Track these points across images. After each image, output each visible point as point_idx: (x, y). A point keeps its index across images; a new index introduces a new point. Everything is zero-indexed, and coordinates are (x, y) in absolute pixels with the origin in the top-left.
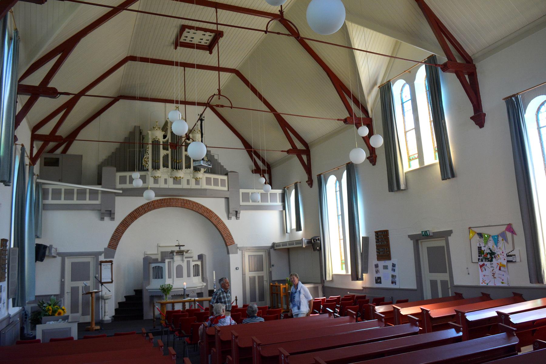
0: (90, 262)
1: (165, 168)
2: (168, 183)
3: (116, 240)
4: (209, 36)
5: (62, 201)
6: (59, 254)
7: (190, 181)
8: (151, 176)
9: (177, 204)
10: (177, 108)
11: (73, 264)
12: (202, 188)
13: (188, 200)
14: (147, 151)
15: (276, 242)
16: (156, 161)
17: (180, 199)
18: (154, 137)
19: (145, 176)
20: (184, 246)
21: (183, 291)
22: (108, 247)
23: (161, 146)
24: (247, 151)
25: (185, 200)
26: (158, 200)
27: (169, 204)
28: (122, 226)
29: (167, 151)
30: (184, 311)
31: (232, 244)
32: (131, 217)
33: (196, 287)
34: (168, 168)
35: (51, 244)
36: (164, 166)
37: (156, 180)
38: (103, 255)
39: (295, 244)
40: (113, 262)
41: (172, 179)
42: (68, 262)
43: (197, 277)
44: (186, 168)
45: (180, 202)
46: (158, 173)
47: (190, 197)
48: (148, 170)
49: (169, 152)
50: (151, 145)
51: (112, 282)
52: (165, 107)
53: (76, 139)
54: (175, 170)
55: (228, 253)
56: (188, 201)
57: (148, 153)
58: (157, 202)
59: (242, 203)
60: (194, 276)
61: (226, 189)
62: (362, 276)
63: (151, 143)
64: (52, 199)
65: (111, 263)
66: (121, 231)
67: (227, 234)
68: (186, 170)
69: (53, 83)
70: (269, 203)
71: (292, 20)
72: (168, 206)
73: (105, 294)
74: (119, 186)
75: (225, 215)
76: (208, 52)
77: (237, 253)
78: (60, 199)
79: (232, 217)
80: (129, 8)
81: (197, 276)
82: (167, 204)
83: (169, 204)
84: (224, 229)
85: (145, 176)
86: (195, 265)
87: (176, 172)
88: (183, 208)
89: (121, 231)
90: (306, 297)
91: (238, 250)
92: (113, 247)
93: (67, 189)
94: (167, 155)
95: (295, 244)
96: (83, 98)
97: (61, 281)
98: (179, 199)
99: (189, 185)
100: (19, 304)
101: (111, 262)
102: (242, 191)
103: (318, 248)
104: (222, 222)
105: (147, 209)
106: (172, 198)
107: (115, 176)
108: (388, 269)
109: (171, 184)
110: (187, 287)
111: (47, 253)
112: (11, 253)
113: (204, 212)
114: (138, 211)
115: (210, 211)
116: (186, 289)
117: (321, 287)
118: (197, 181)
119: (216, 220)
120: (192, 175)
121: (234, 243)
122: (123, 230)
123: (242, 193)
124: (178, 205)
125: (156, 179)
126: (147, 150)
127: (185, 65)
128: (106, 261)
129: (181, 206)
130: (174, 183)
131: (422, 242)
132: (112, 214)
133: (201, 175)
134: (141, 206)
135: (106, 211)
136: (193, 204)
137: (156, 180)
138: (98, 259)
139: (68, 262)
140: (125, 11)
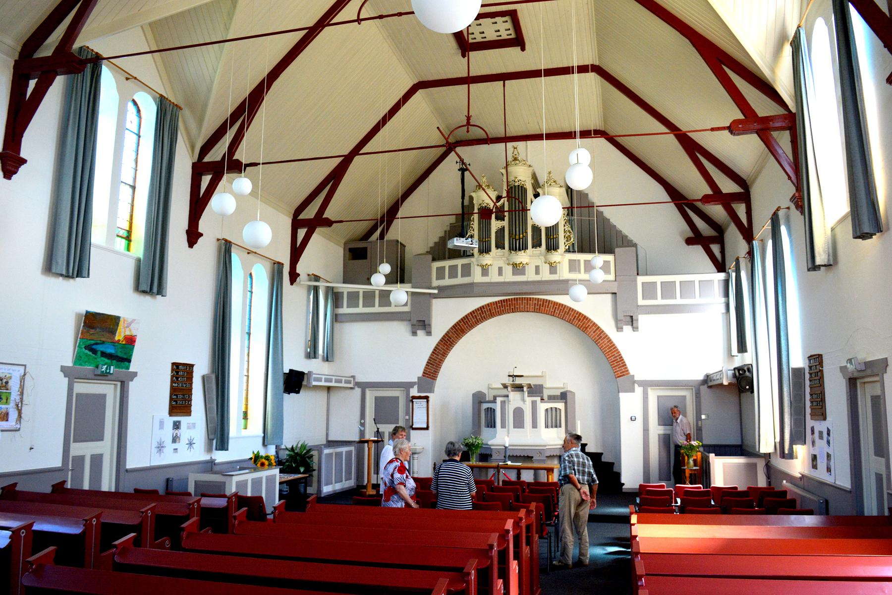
0: (398, 397)
1: (499, 249)
2: (504, 274)
3: (434, 365)
4: (504, 22)
5: (361, 309)
6: (358, 384)
7: (541, 268)
8: (507, 262)
9: (527, 307)
10: (515, 148)
11: (377, 399)
12: (561, 279)
13: (547, 300)
14: (472, 226)
15: (711, 373)
16: (484, 240)
17: (533, 298)
18: (481, 202)
19: (470, 264)
21: (504, 450)
22: (423, 375)
23: (493, 216)
24: (675, 204)
25: (541, 299)
26: (496, 302)
27: (515, 307)
28: (443, 343)
29: (503, 222)
30: (537, 483)
31: (624, 375)
32: (456, 330)
33: (546, 446)
34: (504, 249)
36: (497, 247)
37: (485, 271)
38: (416, 387)
39: (334, 381)
40: (431, 399)
41: (511, 267)
42: (370, 395)
43: (555, 429)
44: (532, 248)
45: (532, 304)
46: (487, 259)
47: (547, 295)
48: (473, 255)
49: (505, 223)
50: (477, 214)
51: (427, 428)
52: (527, 146)
53: (397, 217)
54: (513, 252)
55: (619, 392)
56: (546, 302)
57: (472, 227)
58: (495, 306)
59: (641, 302)
60: (547, 427)
61: (611, 277)
62: (791, 448)
63: (478, 212)
64: (348, 307)
65: (426, 400)
66: (441, 351)
67: (616, 357)
68: (534, 249)
69: (242, 155)
70: (678, 301)
71: (330, 3)
72: (514, 311)
73: (415, 446)
74: (435, 283)
75: (612, 323)
76: (519, 48)
77: (633, 391)
78: (358, 306)
79: (625, 327)
80: (334, 21)
82: (511, 307)
83: (515, 307)
84: (609, 348)
85: (470, 264)
86: (488, 408)
87: (515, 254)
88: (539, 314)
89: (441, 351)
91: (636, 385)
92: (430, 375)
93: (343, 294)
94: (503, 229)
95: (334, 381)
96: (357, 159)
97: (361, 422)
98: (530, 298)
99: (502, 275)
100: (218, 447)
101: (427, 398)
102: (641, 279)
103: (747, 387)
104: (607, 336)
105: (480, 317)
106: (520, 298)
107: (430, 268)
108: (160, 429)
109: (508, 276)
110: (511, 444)
111: (304, 383)
112: (205, 380)
113: (574, 318)
114: (467, 320)
115: (585, 317)
116: (509, 448)
117: (764, 464)
118: (553, 268)
119: (594, 332)
120: (543, 258)
121: (629, 373)
122: (443, 349)
123: (643, 283)
124: (530, 309)
125: (484, 268)
126: (472, 223)
127: (504, 77)
128: (420, 396)
129: (535, 309)
130: (514, 274)
131: (864, 383)
132: (426, 327)
133: (560, 257)
134: (471, 313)
135: (418, 321)
136: (555, 306)
137: (485, 271)
138: (408, 393)
139: (370, 395)
140: (326, 28)
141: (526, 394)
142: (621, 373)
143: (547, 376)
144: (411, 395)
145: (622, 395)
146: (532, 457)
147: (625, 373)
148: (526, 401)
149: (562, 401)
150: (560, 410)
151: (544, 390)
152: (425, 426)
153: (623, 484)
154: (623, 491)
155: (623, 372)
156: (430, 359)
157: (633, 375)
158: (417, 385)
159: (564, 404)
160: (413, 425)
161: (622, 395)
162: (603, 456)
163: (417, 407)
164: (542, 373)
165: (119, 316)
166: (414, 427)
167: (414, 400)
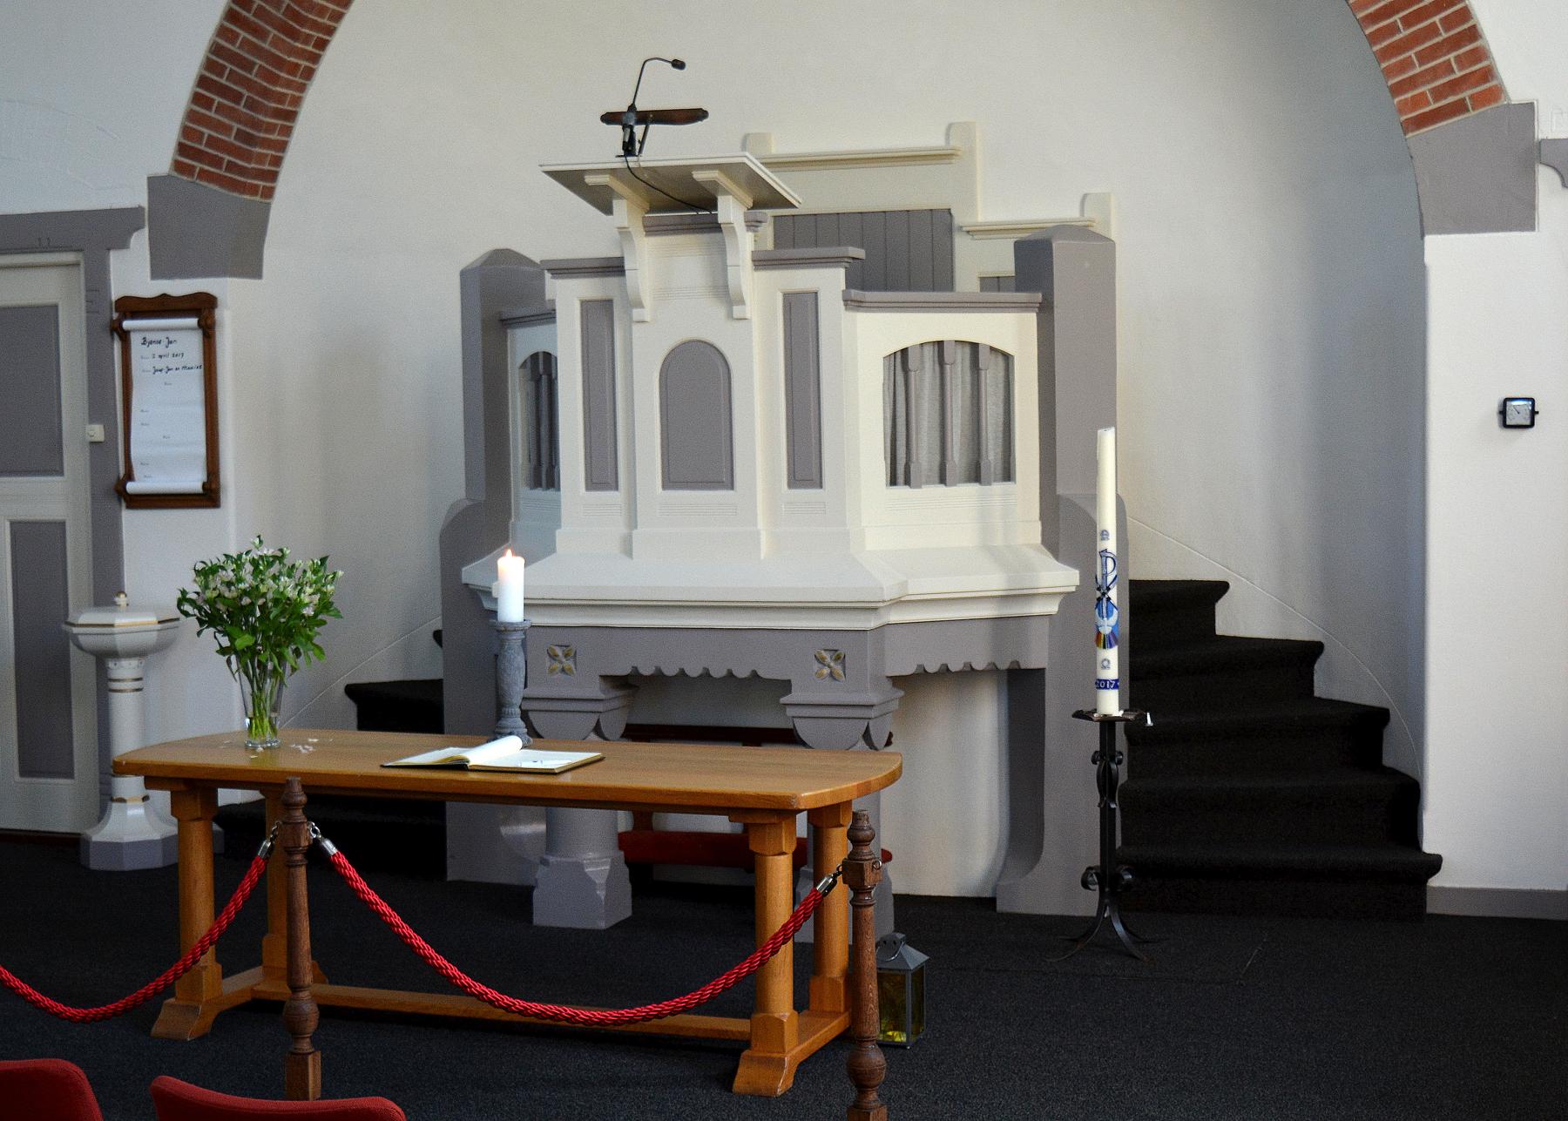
0: (55, 307)
3: (237, 97)
20: (696, 115)
22: (178, 166)
31: (1459, 108)
33: (871, 609)
35: (472, 254)
38: (140, 241)
40: (226, 318)
43: (968, 492)
51: (209, 496)
55: (1423, 236)
60: (899, 473)
65: (193, 321)
81: (975, 475)
90: (236, 905)
92: (217, 162)
121: (1496, 93)
138: (97, 280)
141: (744, 243)
142: (1438, 93)
143: (979, 156)
144: (115, 294)
145: (1441, 250)
146: (786, 686)
147: (1466, 94)
148: (742, 302)
149: (1022, 296)
150: (1007, 358)
151: (961, 243)
152: (193, 481)
153: (1434, 863)
154: (1434, 906)
155: (1454, 86)
156: (217, 58)
157: (1530, 107)
158: (146, 230)
159: (1031, 318)
160: (129, 476)
161: (1441, 250)
162: (1319, 667)
163: (149, 364)
164: (948, 135)
165: (146, 178)
166: (131, 487)
167: (127, 324)
